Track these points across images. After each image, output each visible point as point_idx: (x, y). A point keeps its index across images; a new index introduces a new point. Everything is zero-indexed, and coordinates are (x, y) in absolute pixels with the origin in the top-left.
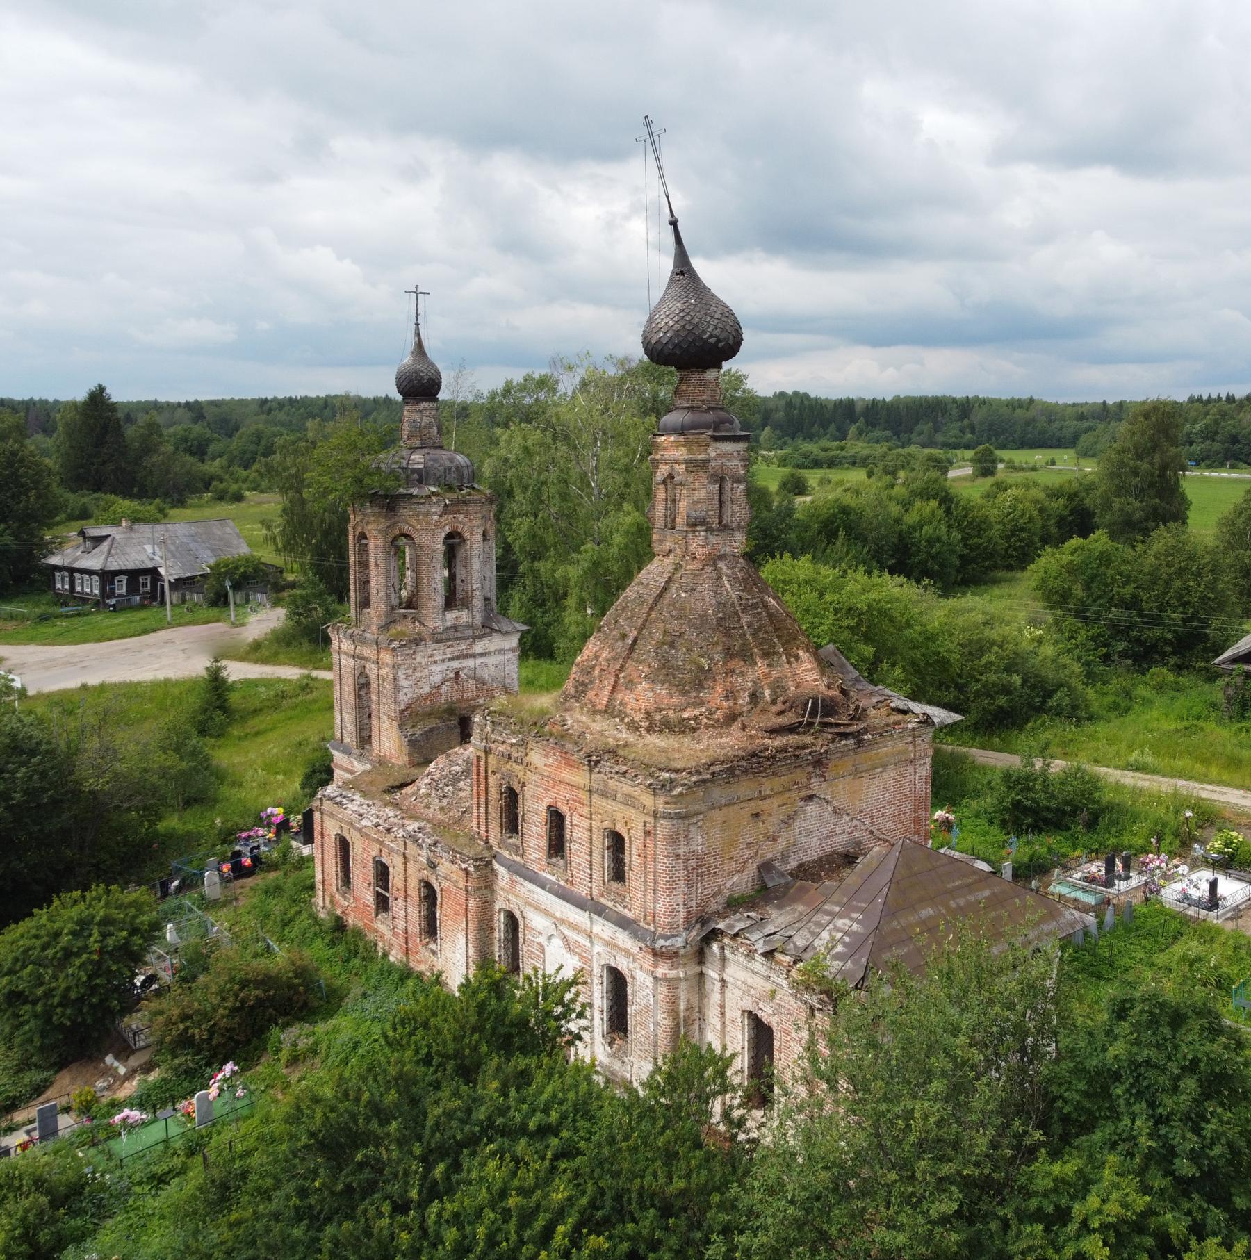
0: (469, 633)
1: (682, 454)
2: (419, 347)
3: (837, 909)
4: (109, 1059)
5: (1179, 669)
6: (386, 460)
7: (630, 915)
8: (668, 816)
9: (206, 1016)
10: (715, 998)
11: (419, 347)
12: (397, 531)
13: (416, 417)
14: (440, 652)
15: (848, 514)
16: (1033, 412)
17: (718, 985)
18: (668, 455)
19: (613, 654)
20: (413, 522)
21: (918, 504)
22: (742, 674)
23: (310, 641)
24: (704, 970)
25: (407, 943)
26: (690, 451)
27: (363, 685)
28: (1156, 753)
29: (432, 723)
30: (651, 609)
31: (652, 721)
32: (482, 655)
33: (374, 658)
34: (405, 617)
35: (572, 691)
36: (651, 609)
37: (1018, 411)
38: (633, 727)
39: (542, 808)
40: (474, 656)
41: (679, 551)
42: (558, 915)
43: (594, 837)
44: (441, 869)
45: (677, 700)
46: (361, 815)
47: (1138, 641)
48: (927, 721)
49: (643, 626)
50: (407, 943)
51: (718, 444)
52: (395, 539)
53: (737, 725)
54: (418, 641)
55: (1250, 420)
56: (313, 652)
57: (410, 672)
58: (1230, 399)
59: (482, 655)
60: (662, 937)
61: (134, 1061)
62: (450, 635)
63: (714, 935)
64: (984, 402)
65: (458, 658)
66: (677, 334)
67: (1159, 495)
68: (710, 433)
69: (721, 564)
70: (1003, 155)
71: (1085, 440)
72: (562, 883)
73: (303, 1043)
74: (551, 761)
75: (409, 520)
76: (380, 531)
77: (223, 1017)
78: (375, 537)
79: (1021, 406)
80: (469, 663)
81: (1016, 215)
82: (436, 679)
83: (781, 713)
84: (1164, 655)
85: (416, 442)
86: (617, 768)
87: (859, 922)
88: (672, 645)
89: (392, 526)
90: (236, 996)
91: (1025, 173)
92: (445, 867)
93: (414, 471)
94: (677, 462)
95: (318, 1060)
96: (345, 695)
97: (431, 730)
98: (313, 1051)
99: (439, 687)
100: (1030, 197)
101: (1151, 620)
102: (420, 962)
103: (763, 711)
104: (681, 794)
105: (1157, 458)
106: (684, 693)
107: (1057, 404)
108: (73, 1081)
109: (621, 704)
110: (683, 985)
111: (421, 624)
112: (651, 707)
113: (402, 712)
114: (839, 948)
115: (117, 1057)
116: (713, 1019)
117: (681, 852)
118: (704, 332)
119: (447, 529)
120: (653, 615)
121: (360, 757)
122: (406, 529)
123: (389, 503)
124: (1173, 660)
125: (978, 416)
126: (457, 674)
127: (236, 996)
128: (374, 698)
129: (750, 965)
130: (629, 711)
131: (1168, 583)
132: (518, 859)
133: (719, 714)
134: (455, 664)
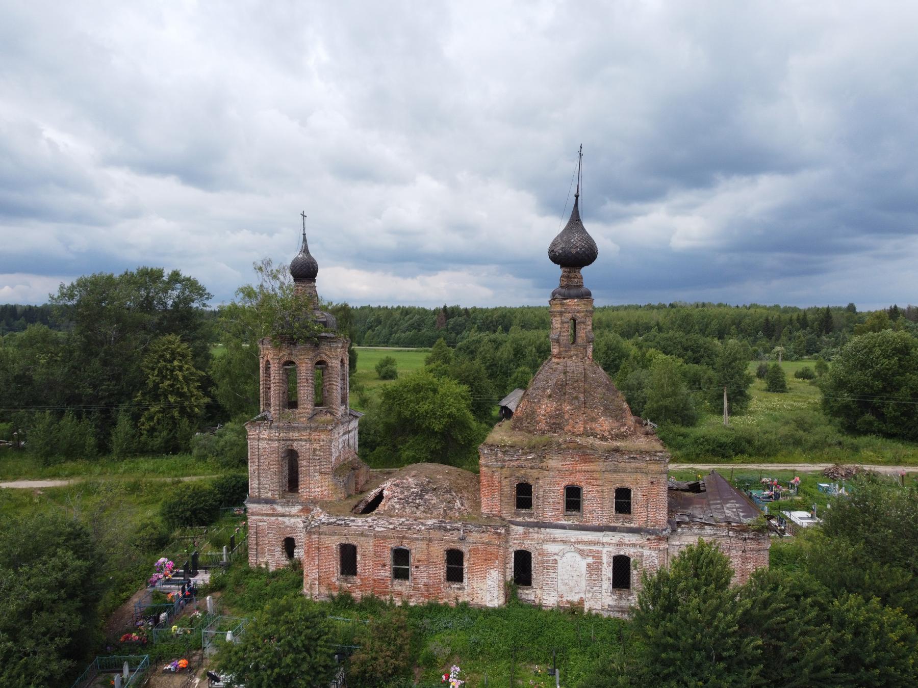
11: (306, 251)
12: (319, 359)
18: (569, 309)
27: (291, 458)
38: (603, 438)
39: (560, 490)
42: (573, 540)
44: (470, 539)
45: (617, 424)
72: (577, 523)
74: (568, 462)
78: (307, 363)
81: (115, 199)
89: (316, 356)
91: (119, 175)
94: (578, 312)
100: (121, 186)
106: (618, 421)
111: (332, 414)
122: (324, 358)
132: (532, 520)
134: (346, 437)
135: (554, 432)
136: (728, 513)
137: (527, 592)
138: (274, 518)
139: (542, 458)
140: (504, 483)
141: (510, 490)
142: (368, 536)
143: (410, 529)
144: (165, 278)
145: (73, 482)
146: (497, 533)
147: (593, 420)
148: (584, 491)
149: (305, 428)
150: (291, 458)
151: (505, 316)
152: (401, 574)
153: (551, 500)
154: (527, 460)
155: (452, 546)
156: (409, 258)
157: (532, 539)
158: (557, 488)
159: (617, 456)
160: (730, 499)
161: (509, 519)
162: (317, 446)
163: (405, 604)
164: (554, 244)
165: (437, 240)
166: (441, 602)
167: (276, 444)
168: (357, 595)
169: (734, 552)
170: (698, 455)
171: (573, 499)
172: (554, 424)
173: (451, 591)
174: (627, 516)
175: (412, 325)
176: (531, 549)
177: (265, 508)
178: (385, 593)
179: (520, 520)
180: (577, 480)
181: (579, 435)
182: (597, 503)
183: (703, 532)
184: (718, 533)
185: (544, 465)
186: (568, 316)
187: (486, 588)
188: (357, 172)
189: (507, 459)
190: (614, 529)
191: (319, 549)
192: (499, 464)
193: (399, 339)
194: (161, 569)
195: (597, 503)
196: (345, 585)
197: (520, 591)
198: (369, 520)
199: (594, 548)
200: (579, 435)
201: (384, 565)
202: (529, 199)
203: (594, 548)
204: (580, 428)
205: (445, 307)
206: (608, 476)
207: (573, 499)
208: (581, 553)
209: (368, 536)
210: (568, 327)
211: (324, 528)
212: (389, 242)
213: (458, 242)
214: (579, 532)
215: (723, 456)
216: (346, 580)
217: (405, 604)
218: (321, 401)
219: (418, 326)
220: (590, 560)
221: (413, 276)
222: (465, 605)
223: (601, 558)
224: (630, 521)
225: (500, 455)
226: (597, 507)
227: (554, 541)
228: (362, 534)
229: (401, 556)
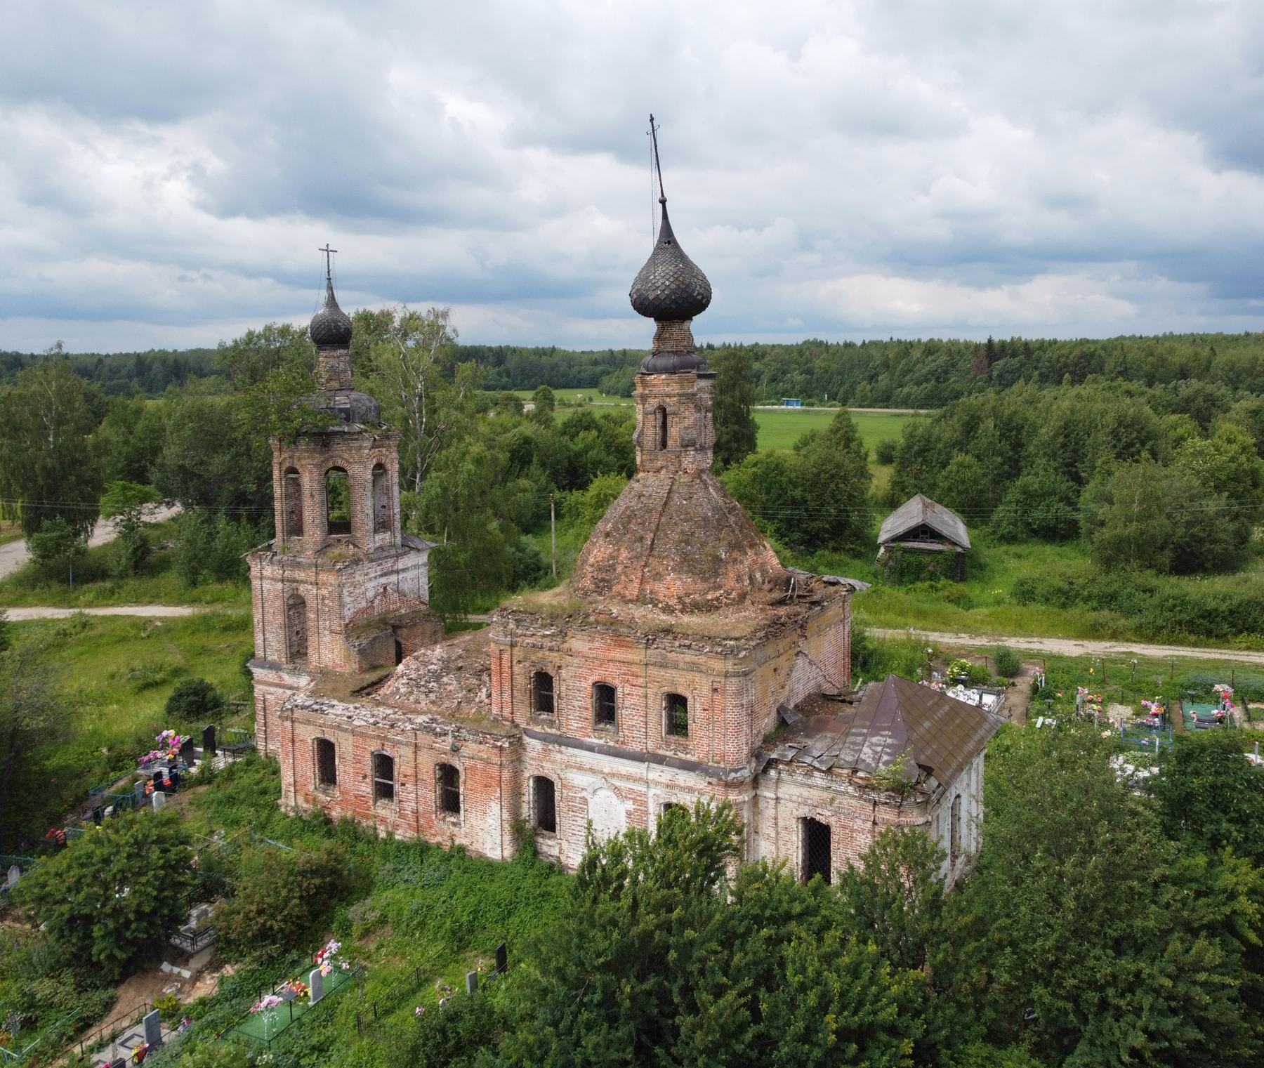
0: (393, 552)
1: (674, 389)
2: (332, 303)
3: (865, 731)
4: (166, 967)
5: (835, 550)
6: (316, 401)
7: (694, 759)
8: (737, 675)
9: (277, 908)
10: (770, 812)
11: (332, 303)
12: (331, 465)
13: (332, 362)
14: (374, 570)
15: (530, 443)
16: (555, 360)
17: (773, 802)
18: (656, 390)
19: (633, 553)
20: (346, 456)
21: (581, 434)
22: (741, 562)
23: (60, 581)
24: (759, 792)
25: (417, 821)
26: (682, 387)
27: (296, 605)
28: (869, 611)
29: (374, 633)
30: (661, 515)
31: (684, 604)
32: (403, 570)
33: (313, 579)
34: (339, 541)
35: (592, 587)
36: (661, 515)
37: (544, 358)
38: (668, 610)
39: (587, 686)
40: (398, 572)
41: (672, 468)
42: (606, 770)
43: (650, 701)
44: (465, 751)
45: (700, 586)
46: (350, 717)
47: (805, 532)
48: (852, 589)
49: (657, 529)
50: (417, 821)
52: (327, 472)
53: (748, 602)
54: (357, 561)
55: (1263, 354)
56: (65, 592)
57: (352, 589)
58: (710, 347)
59: (403, 570)
60: (732, 771)
61: (196, 964)
62: (379, 555)
63: (771, 763)
64: (514, 350)
66: (673, 292)
67: (737, 423)
68: (694, 371)
69: (704, 477)
70: (521, 139)
71: (606, 382)
72: (611, 744)
73: (372, 917)
74: (597, 645)
75: (341, 454)
76: (315, 466)
77: (296, 905)
78: (310, 471)
79: (545, 354)
80: (393, 578)
81: (532, 191)
82: (371, 594)
83: (771, 590)
84: (823, 540)
85: (335, 385)
86: (677, 643)
87: (890, 737)
88: (687, 543)
89: (327, 460)
90: (300, 886)
91: (538, 157)
92: (470, 748)
93: (341, 410)
94: (668, 396)
95: (389, 928)
96: (269, 617)
97: (374, 639)
98: (383, 921)
99: (372, 602)
100: (542, 175)
101: (812, 516)
102: (435, 835)
103: (760, 589)
104: (745, 657)
105: (737, 393)
106: (705, 580)
107: (574, 352)
108: (139, 993)
109: (651, 592)
110: (746, 807)
111: (355, 546)
112: (682, 593)
113: (347, 625)
114: (885, 758)
115: (174, 963)
116: (767, 828)
117: (744, 702)
118: (694, 291)
119: (375, 461)
120: (663, 519)
121: (295, 671)
122: (340, 463)
123: (324, 439)
124: (831, 544)
125: (511, 363)
126: (385, 588)
127: (300, 886)
128: (312, 616)
129: (810, 782)
130: (661, 598)
131: (825, 486)
132: (554, 731)
133: (734, 594)
134: (383, 580)
135: (600, 594)
136: (867, 753)
137: (550, 842)
138: (281, 690)
139: (563, 634)
140: (517, 669)
141: (523, 680)
142: (346, 731)
143: (392, 726)
144: (397, 324)
145: (184, 611)
146: (496, 747)
147: (658, 577)
148: (619, 694)
149: (309, 566)
150: (296, 605)
151: (1092, 355)
152: (385, 792)
153: (576, 703)
154: (544, 636)
155: (444, 758)
156: (977, 256)
157: (553, 762)
158: (584, 684)
159: (666, 642)
160: (885, 729)
161: (524, 726)
162: (324, 592)
163: (390, 835)
164: (643, 278)
165: (1022, 223)
166: (433, 841)
167: (279, 586)
168: (336, 814)
169: (859, 822)
170: (1159, 629)
171: (605, 703)
172: (603, 580)
173: (445, 827)
174: (681, 740)
175: (932, 373)
176: (553, 778)
177: (271, 676)
178: (367, 817)
179: (538, 729)
180: (611, 675)
181: (631, 601)
182: (640, 716)
183: (810, 782)
184: (834, 786)
185: (566, 646)
186: (653, 403)
187: (486, 830)
188: (874, 122)
189: (519, 632)
190: (660, 760)
191: (293, 741)
192: (509, 639)
193: (908, 396)
194: (164, 745)
195: (640, 716)
196: (321, 797)
197: (540, 840)
198: (351, 707)
199: (635, 787)
200: (631, 601)
201: (365, 777)
202: (1193, 143)
203: (635, 787)
204: (633, 590)
205: (990, 341)
206: (652, 671)
207: (605, 703)
208: (617, 791)
209: (346, 731)
210: (654, 422)
211: (298, 714)
212: (940, 232)
213: (1061, 225)
214: (612, 759)
215: (1209, 633)
216: (325, 792)
217: (390, 835)
218: (340, 527)
219: (940, 376)
220: (630, 805)
221: (995, 285)
222: (462, 849)
223: (645, 804)
224: (686, 750)
225: (512, 626)
226: (637, 721)
227: (581, 768)
228: (339, 727)
229: (384, 765)
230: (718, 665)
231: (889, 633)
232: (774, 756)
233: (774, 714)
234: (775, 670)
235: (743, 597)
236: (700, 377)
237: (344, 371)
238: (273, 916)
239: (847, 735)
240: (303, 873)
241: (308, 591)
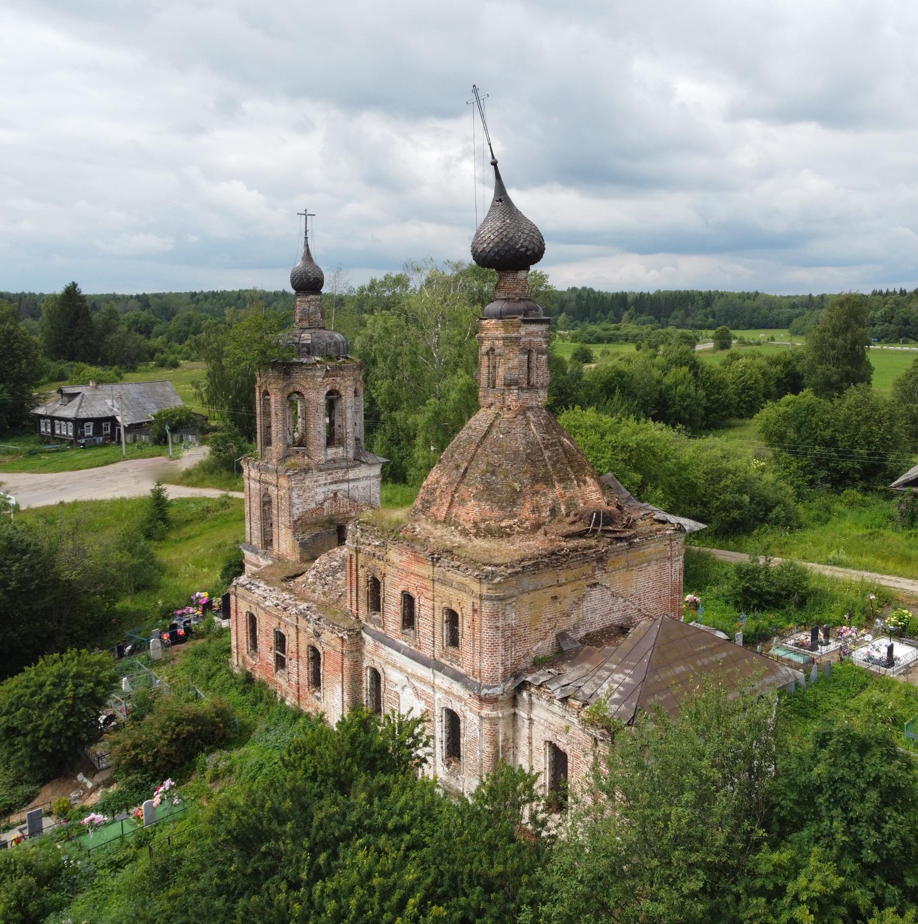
0: (344, 464)
1: (500, 333)
2: (308, 255)
3: (614, 667)
4: (80, 777)
5: (865, 490)
6: (283, 337)
7: (462, 671)
8: (490, 599)
10: (525, 732)
11: (308, 255)
12: (291, 390)
13: (305, 306)
14: (323, 478)
15: (622, 377)
16: (758, 302)
17: (527, 722)
18: (490, 334)
19: (450, 479)
20: (303, 383)
21: (673, 370)
23: (227, 470)
24: (517, 711)
25: (298, 691)
26: (506, 331)
27: (266, 503)
28: (848, 553)
29: (317, 530)
30: (478, 446)
31: (478, 529)
32: (354, 480)
33: (275, 482)
34: (297, 452)
35: (420, 507)
36: (478, 446)
37: (747, 301)
38: (465, 533)
39: (398, 592)
40: (348, 481)
41: (498, 404)
42: (409, 671)
44: (324, 638)
45: (497, 513)
47: (835, 470)
49: (472, 459)
50: (298, 691)
51: (527, 326)
52: (290, 396)
53: (541, 532)
54: (306, 470)
55: (917, 308)
56: (229, 478)
57: (301, 493)
58: (903, 293)
59: (354, 480)
60: (486, 687)
61: (99, 778)
62: (330, 466)
63: (524, 685)
64: (722, 295)
65: (336, 482)
66: (497, 245)
67: (850, 363)
68: (521, 317)
69: (529, 414)
70: (736, 114)
72: (412, 647)
74: (404, 558)
75: (300, 381)
76: (279, 389)
78: (275, 394)
79: (749, 298)
80: (344, 486)
81: (746, 158)
82: (320, 498)
83: (573, 523)
84: (854, 480)
85: (306, 324)
88: (493, 473)
89: (288, 386)
91: (752, 127)
92: (327, 636)
93: (304, 345)
94: (497, 339)
95: (233, 778)
96: (253, 510)
97: (317, 535)
98: (230, 771)
99: (322, 504)
100: (756, 145)
101: (845, 455)
102: (308, 706)
103: (560, 521)
104: (499, 583)
105: (849, 336)
106: (502, 508)
107: (776, 297)
108: (54, 793)
109: (456, 516)
110: (501, 723)
111: (309, 457)
112: (478, 519)
113: (295, 522)
114: (616, 696)
115: (86, 775)
116: (523, 747)
117: (500, 625)
119: (328, 388)
120: (479, 451)
122: (298, 388)
123: (286, 369)
124: (861, 484)
125: (717, 305)
126: (335, 494)
127: (173, 730)
128: (275, 512)
129: (550, 708)
130: (461, 522)
132: (380, 630)
133: (527, 524)
134: (334, 487)
230: (475, 587)
231: (828, 571)
232: (529, 679)
233: (551, 638)
234: (555, 598)
235: (537, 526)
236: (525, 322)
237: (315, 313)
238: (146, 751)
239: (600, 668)
240: (179, 722)
241: (272, 490)
